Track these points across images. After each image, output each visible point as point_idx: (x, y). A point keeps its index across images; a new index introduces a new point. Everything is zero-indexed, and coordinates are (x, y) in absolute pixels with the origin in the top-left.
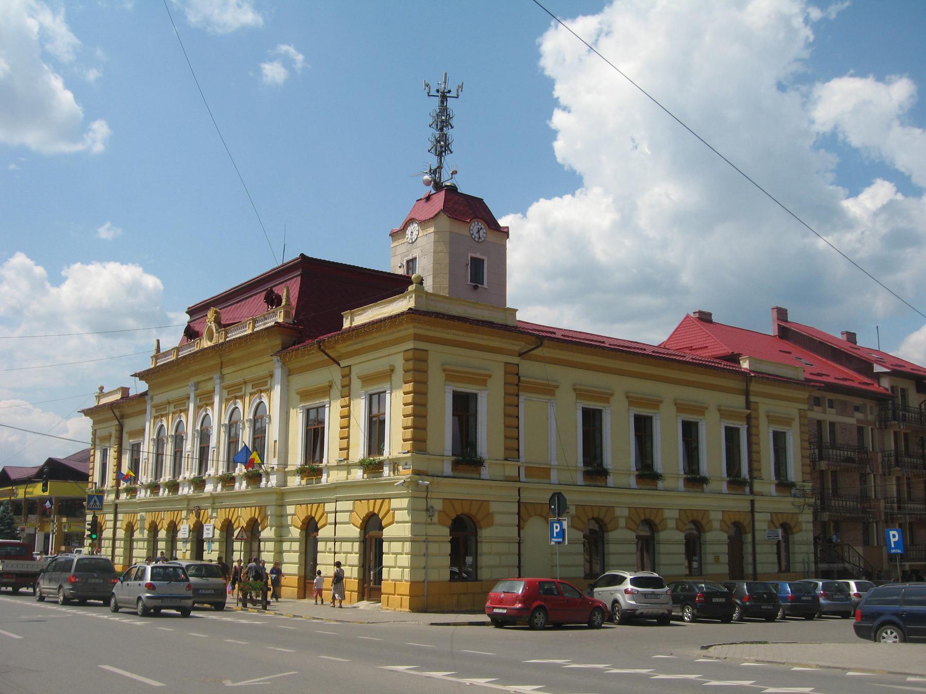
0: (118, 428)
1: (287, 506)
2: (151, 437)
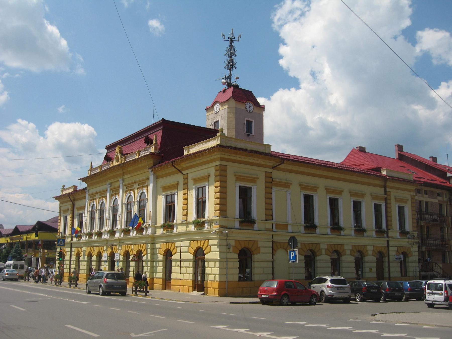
0: (72, 206)
2: (88, 210)
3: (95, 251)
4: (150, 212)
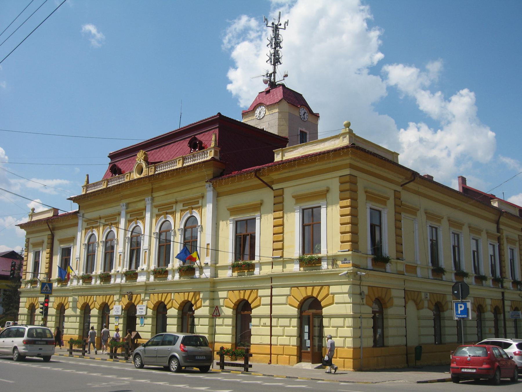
0: (50, 237)
1: (219, 292)
2: (83, 242)
3: (96, 301)
4: (208, 244)
